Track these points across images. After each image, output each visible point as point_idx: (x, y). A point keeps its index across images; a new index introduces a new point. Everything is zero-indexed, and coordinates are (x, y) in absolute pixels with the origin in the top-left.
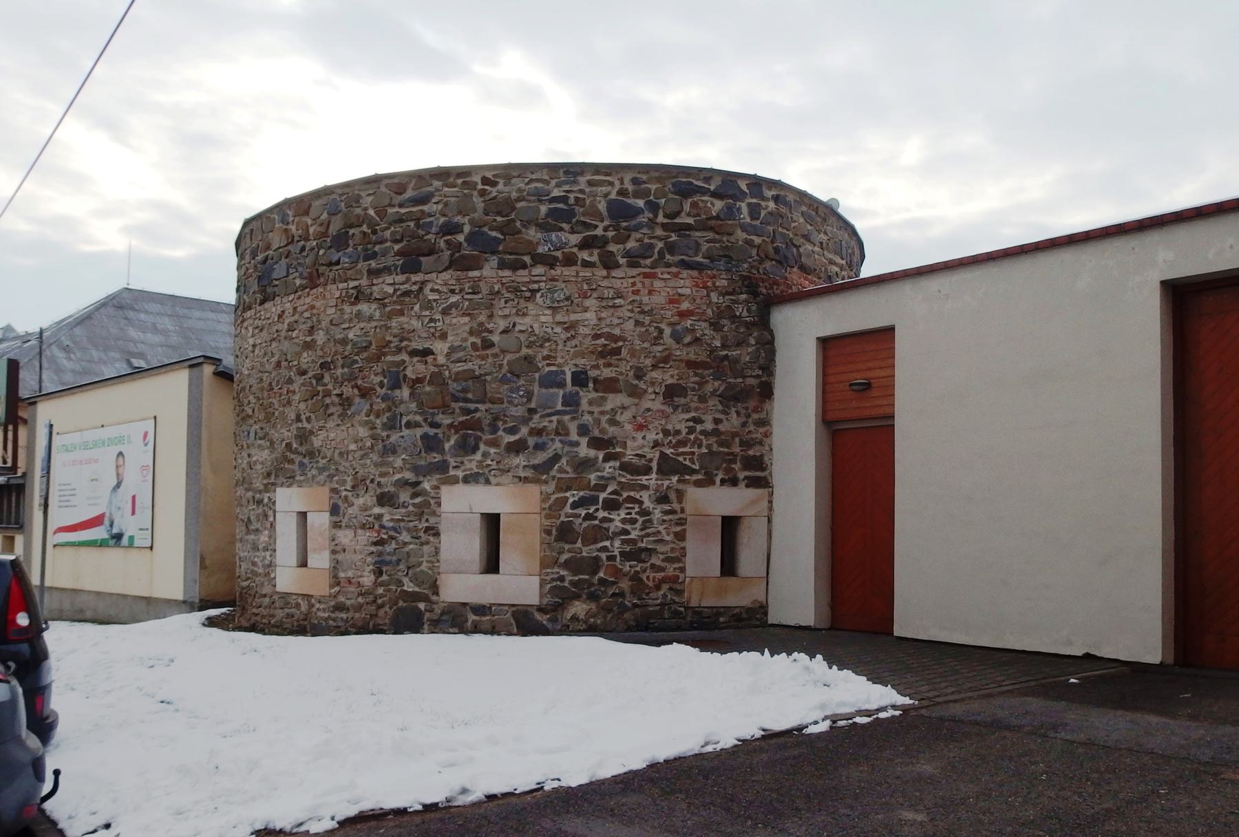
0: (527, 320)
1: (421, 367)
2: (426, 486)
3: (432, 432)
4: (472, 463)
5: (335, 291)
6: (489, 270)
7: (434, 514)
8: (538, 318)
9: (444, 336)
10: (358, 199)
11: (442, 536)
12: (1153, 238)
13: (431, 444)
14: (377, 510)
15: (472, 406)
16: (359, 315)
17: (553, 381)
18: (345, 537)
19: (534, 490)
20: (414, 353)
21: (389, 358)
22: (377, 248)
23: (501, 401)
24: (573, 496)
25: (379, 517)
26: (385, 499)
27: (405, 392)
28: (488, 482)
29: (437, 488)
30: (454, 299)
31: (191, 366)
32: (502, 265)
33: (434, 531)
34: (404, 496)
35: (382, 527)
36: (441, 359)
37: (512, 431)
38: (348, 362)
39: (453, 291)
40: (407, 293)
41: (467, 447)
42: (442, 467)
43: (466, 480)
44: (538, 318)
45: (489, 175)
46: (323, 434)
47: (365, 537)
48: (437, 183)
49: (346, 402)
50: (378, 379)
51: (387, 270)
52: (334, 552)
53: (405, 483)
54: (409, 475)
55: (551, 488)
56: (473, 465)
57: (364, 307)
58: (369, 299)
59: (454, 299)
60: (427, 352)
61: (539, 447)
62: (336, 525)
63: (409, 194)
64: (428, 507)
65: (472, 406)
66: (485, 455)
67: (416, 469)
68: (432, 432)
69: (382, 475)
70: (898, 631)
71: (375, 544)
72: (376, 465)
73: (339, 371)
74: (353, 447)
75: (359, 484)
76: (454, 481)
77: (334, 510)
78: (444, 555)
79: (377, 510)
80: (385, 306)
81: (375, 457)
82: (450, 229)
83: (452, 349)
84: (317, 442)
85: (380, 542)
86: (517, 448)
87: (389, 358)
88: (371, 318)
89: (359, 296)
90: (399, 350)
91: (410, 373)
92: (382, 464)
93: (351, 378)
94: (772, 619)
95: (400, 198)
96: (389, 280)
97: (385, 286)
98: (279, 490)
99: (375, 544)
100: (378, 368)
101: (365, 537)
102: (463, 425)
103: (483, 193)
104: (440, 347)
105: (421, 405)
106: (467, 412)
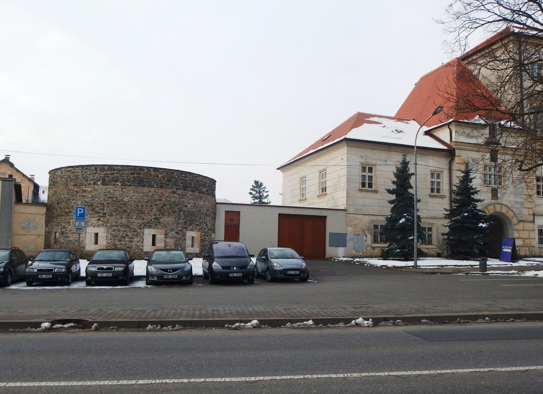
0: (201, 203)
1: (186, 209)
2: (184, 231)
3: (186, 221)
4: (191, 227)
5: (169, 190)
6: (196, 193)
7: (185, 236)
8: (201, 203)
9: (190, 204)
10: (173, 173)
11: (187, 240)
12: (278, 208)
13: (185, 223)
14: (175, 235)
15: (192, 217)
16: (174, 196)
17: (203, 214)
18: (168, 240)
19: (199, 233)
20: (184, 206)
21: (180, 206)
22: (177, 184)
23: (196, 217)
24: (203, 234)
25: (176, 236)
26: (177, 233)
27: (182, 213)
28: (193, 231)
29: (186, 231)
30: (192, 197)
31: (2, 180)
32: (198, 193)
33: (185, 239)
34: (180, 233)
35: (177, 238)
36: (189, 208)
37: (197, 222)
38: (170, 205)
39: (191, 196)
40: (184, 194)
41: (191, 224)
42: (187, 228)
43: (190, 230)
44: (201, 203)
45: (197, 176)
46: (163, 219)
47: (173, 240)
48: (188, 175)
49: (169, 213)
50: (177, 210)
51: (180, 189)
52: (165, 243)
53: (180, 230)
54: (181, 229)
55: (201, 232)
56: (191, 228)
57: (176, 195)
58: (176, 194)
59: (192, 197)
60: (187, 206)
61: (200, 225)
62: (165, 237)
63: (183, 175)
64: (184, 235)
65: (192, 217)
66: (193, 226)
67: (183, 228)
68: (186, 221)
69: (177, 228)
70: (146, 275)
71: (175, 241)
72: (175, 226)
73: (168, 207)
74: (171, 222)
75: (172, 230)
76: (188, 230)
77: (166, 234)
78: (187, 244)
79: (175, 235)
80: (180, 196)
81: (175, 225)
82: (190, 184)
83: (191, 206)
84: (161, 220)
85: (176, 241)
86: (197, 225)
87: (180, 206)
88: (177, 198)
89: (174, 193)
90: (181, 205)
91: (184, 209)
92: (177, 226)
93: (171, 208)
94: (202, 259)
95: (182, 175)
96: (181, 191)
97: (180, 192)
98: (145, 229)
99: (175, 241)
100: (178, 207)
101: (173, 240)
102: (191, 220)
103: (195, 179)
104: (189, 206)
105: (185, 216)
106: (191, 218)
